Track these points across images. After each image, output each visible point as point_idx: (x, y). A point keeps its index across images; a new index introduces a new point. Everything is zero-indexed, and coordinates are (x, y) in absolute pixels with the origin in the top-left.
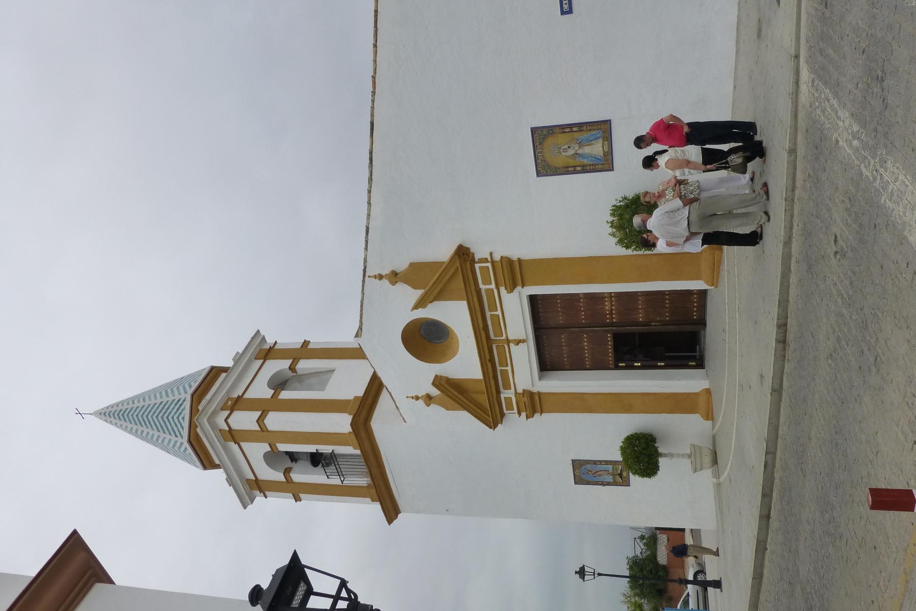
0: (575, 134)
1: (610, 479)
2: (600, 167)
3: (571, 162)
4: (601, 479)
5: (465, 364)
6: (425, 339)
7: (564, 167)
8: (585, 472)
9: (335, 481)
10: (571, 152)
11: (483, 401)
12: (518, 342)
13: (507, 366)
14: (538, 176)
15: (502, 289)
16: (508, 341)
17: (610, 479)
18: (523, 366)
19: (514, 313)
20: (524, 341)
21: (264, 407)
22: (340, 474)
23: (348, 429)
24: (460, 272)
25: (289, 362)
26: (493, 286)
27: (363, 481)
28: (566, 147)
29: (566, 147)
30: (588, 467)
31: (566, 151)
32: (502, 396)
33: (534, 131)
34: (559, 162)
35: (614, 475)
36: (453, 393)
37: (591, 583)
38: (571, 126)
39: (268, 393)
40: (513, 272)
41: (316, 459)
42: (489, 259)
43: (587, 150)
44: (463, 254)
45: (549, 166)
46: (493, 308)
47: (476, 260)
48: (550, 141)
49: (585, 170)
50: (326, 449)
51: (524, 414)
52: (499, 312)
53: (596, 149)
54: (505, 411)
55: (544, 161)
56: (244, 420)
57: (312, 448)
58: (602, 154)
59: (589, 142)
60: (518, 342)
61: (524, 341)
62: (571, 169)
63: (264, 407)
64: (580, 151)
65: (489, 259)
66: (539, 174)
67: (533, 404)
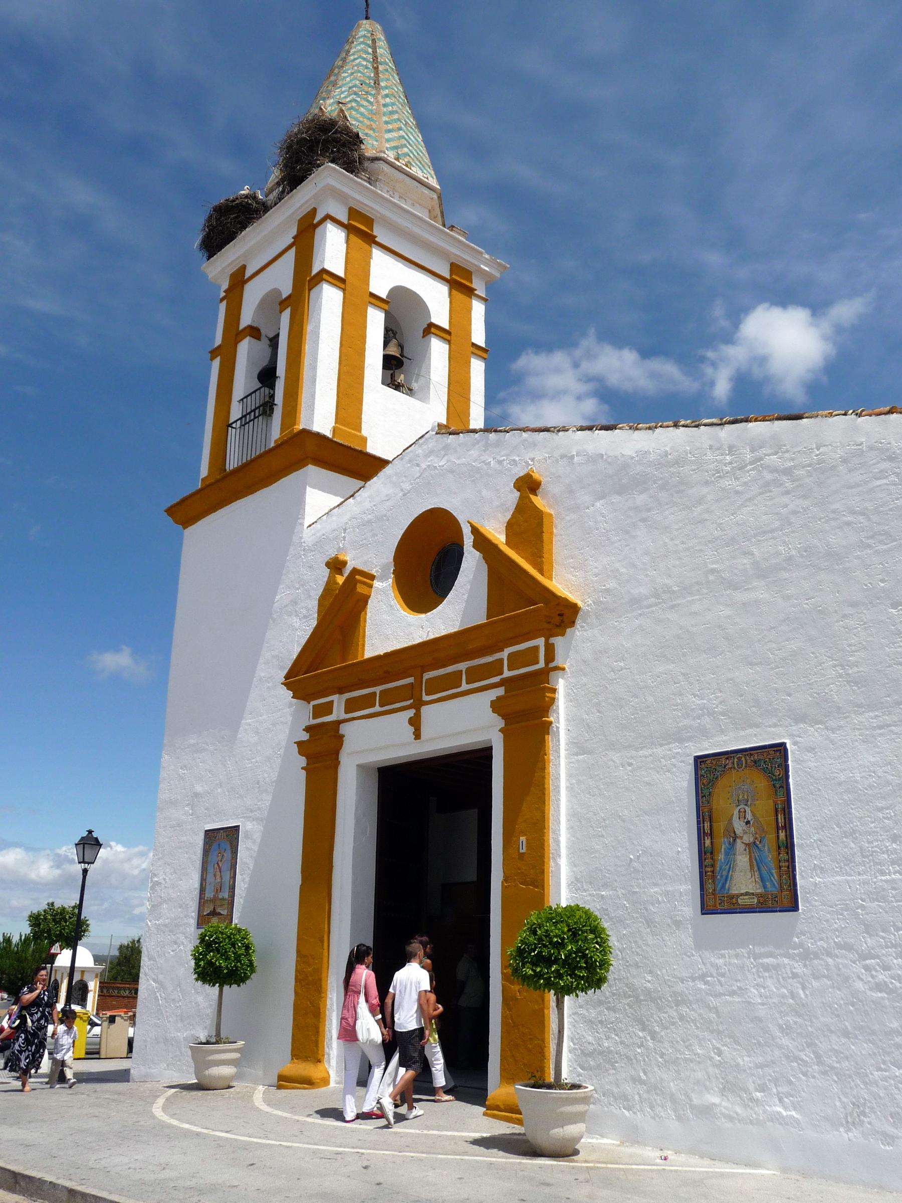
0: (773, 836)
1: (209, 894)
2: (709, 887)
3: (720, 827)
4: (211, 870)
5: (391, 626)
6: (429, 556)
7: (710, 811)
8: (221, 843)
9: (236, 412)
10: (739, 826)
11: (329, 667)
12: (415, 722)
13: (381, 706)
14: (697, 758)
15: (501, 691)
16: (418, 704)
17: (209, 894)
18: (378, 739)
19: (462, 721)
20: (417, 735)
21: (352, 284)
22: (245, 419)
23: (358, 585)
24: (530, 612)
25: (445, 323)
26: (507, 673)
27: (233, 462)
28: (749, 817)
29: (749, 817)
30: (228, 855)
31: (741, 820)
32: (335, 698)
33: (781, 749)
34: (721, 801)
35: (214, 900)
36: (343, 603)
37: (369, 15)
38: (788, 826)
39: (380, 286)
40: (527, 712)
41: (267, 376)
42: (552, 665)
43: (742, 860)
44: (563, 615)
45: (712, 782)
46: (474, 675)
47: (552, 640)
48: (761, 783)
49: (706, 856)
50: (280, 386)
51: (305, 737)
52: (465, 686)
53: (744, 881)
54: (313, 703)
55: (725, 770)
56: (333, 249)
57: (281, 370)
58: (734, 891)
59: (756, 864)
60: (415, 722)
61: (417, 735)
62: (707, 825)
63: (352, 284)
64: (739, 846)
65: (552, 665)
66: (699, 761)
67: (320, 751)
